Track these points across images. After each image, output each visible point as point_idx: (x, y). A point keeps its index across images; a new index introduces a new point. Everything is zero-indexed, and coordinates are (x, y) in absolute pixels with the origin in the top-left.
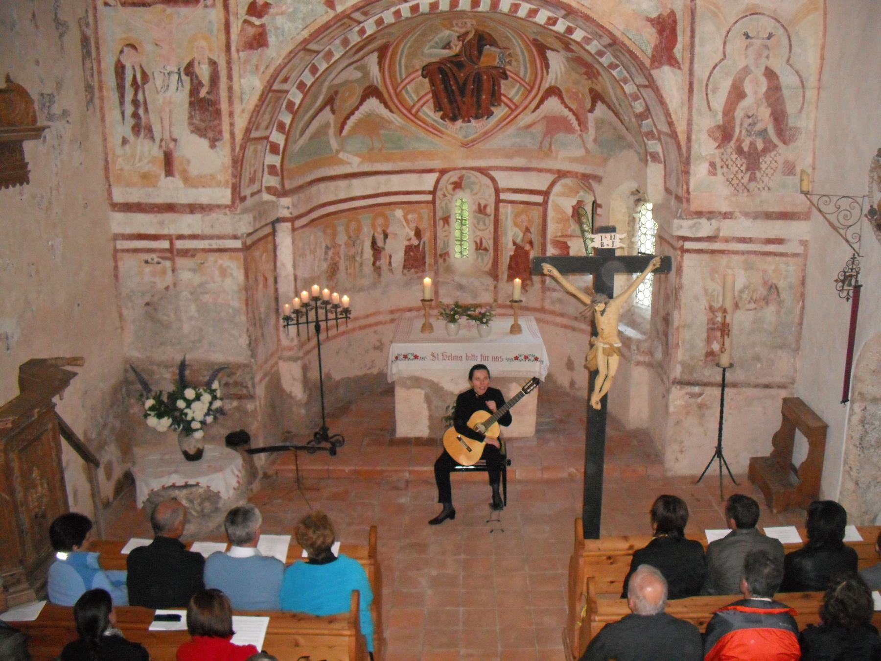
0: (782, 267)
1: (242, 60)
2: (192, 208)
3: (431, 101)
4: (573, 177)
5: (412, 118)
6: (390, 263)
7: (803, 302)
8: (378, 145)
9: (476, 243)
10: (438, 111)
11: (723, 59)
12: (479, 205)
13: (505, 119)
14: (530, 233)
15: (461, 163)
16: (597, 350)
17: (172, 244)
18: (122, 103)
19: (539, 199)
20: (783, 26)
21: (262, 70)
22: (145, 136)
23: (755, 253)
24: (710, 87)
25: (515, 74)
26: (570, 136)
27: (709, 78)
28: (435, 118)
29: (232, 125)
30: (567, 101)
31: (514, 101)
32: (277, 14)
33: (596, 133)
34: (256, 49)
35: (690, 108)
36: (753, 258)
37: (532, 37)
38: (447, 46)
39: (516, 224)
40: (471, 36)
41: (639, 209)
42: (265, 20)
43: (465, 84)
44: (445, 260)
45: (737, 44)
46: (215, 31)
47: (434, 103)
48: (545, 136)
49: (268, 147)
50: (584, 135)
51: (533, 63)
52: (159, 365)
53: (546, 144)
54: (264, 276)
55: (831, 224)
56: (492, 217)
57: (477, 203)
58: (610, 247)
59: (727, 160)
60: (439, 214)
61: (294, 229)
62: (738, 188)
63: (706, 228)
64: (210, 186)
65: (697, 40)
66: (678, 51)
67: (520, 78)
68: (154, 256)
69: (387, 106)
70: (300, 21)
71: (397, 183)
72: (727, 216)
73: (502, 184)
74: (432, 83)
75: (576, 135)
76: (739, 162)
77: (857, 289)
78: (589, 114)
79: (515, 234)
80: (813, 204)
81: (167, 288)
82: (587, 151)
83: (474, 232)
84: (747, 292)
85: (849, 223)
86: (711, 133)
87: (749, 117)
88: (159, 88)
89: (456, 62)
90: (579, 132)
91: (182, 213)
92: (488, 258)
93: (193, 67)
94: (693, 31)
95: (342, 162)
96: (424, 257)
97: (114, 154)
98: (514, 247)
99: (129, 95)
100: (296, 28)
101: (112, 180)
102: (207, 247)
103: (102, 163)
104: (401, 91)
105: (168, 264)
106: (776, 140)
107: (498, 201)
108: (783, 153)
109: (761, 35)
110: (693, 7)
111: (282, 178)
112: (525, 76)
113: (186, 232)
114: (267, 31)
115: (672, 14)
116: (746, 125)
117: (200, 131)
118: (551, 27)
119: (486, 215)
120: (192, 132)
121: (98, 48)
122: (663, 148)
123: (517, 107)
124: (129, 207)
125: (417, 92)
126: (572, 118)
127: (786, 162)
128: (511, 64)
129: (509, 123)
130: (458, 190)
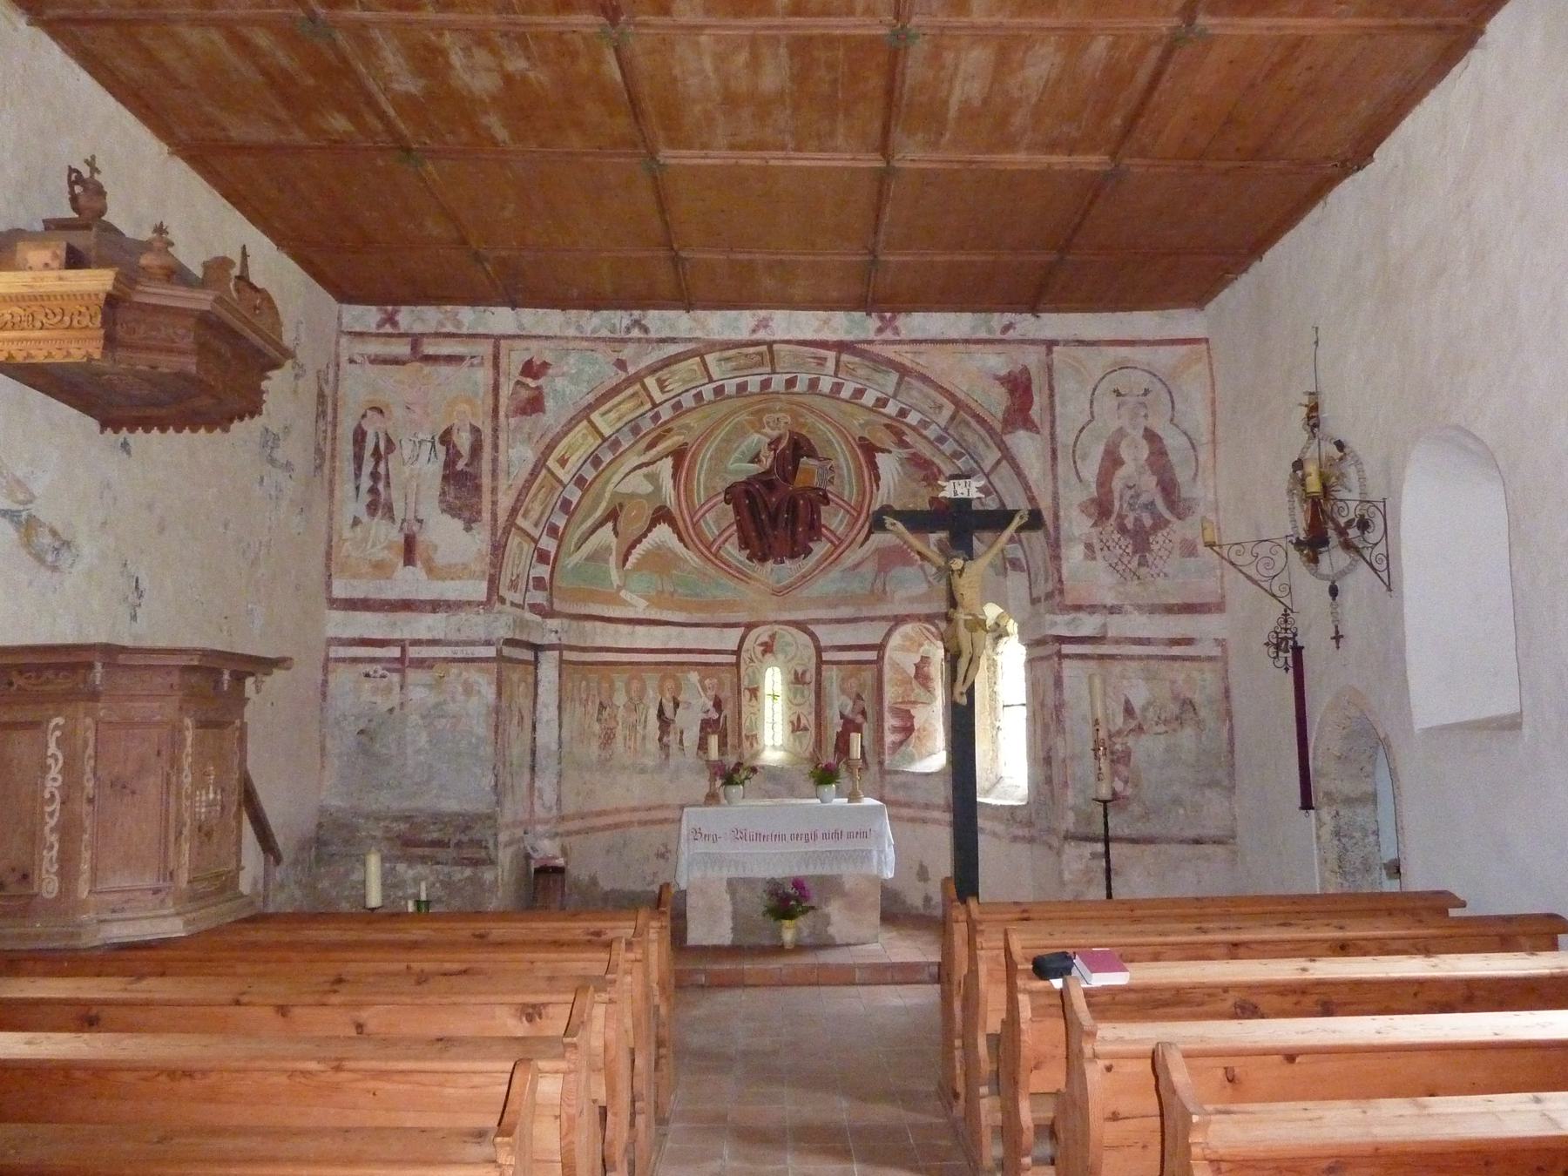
0: (1195, 674)
1: (512, 427)
2: (435, 606)
5: (712, 557)
7: (1231, 721)
8: (669, 588)
9: (792, 723)
11: (1091, 421)
12: (796, 673)
15: (772, 616)
16: (957, 623)
17: (403, 651)
18: (358, 475)
19: (871, 655)
20: (1160, 380)
21: (535, 440)
22: (384, 515)
23: (1156, 657)
24: (1078, 453)
25: (837, 497)
27: (1076, 443)
28: (742, 559)
29: (494, 503)
31: (838, 533)
35: (1055, 478)
36: (1153, 664)
37: (859, 433)
38: (756, 459)
39: (843, 691)
42: (541, 382)
43: (778, 509)
44: (752, 745)
45: (1107, 403)
46: (481, 394)
49: (535, 555)
51: (860, 476)
52: (367, 817)
53: (879, 584)
54: (520, 712)
55: (1249, 577)
56: (813, 684)
57: (793, 672)
58: (965, 496)
59: (1108, 541)
60: (745, 682)
61: (562, 661)
62: (1125, 575)
63: (1088, 625)
64: (460, 578)
65: (1057, 399)
66: (1035, 412)
67: (845, 502)
68: (378, 667)
69: (681, 539)
70: (585, 384)
71: (691, 638)
72: (1113, 610)
73: (825, 641)
74: (737, 512)
75: (916, 567)
76: (1123, 542)
77: (1298, 651)
80: (1223, 558)
81: (391, 710)
83: (790, 709)
84: (1151, 709)
85: (1272, 573)
86: (1084, 509)
87: (1130, 488)
88: (406, 458)
89: (765, 481)
90: (920, 562)
91: (421, 611)
94: (1051, 389)
95: (624, 603)
97: (340, 537)
99: (368, 467)
101: (333, 570)
102: (450, 655)
103: (323, 547)
104: (699, 520)
105: (395, 678)
106: (1167, 515)
107: (820, 663)
108: (1179, 530)
109: (1136, 392)
111: (551, 594)
113: (424, 635)
115: (1025, 370)
116: (1127, 497)
117: (451, 510)
119: (804, 683)
120: (443, 511)
121: (335, 410)
122: (1025, 552)
123: (841, 541)
124: (352, 605)
125: (717, 522)
127: (1184, 541)
128: (832, 483)
130: (768, 655)
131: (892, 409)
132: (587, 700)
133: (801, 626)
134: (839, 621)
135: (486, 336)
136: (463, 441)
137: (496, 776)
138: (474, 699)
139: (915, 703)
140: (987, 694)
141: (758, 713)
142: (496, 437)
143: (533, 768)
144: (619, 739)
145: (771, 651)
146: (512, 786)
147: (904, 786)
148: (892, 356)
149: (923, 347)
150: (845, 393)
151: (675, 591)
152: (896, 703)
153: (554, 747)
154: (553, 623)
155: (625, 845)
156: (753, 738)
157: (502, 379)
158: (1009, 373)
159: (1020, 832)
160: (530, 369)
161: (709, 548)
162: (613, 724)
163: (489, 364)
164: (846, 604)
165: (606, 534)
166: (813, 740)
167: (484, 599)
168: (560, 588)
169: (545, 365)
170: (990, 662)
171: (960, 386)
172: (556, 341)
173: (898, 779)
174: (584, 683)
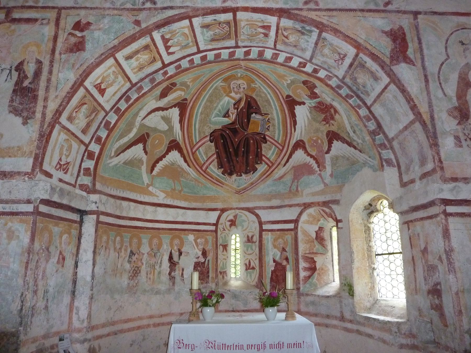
1: (63, 60)
3: (216, 160)
4: (316, 206)
5: (203, 173)
6: (182, 274)
8: (178, 188)
9: (246, 264)
10: (220, 168)
11: (446, 60)
12: (248, 237)
13: (265, 174)
14: (286, 251)
15: (235, 205)
19: (291, 226)
21: (76, 68)
24: (441, 78)
26: (312, 177)
28: (219, 173)
29: (45, 107)
30: (309, 149)
31: (271, 160)
32: (95, 30)
33: (332, 168)
34: (75, 53)
35: (428, 93)
37: (286, 92)
38: (226, 115)
39: (275, 247)
40: (242, 104)
41: (372, 220)
44: (223, 277)
45: (454, 49)
47: (218, 162)
48: (293, 182)
50: (323, 173)
53: (294, 187)
56: (257, 243)
57: (246, 236)
60: (220, 241)
61: (98, 222)
65: (424, 46)
66: (410, 52)
69: (186, 161)
71: (190, 216)
73: (263, 219)
74: (216, 147)
78: (327, 156)
79: (274, 253)
82: (326, 185)
83: (244, 256)
86: (450, 113)
90: (319, 172)
92: (255, 274)
93: (22, 65)
95: (151, 194)
96: (208, 272)
98: (275, 264)
100: (109, 39)
104: (195, 151)
107: (261, 230)
110: (417, 24)
112: (278, 138)
114: (86, 40)
115: (401, 28)
117: (15, 111)
118: (302, 69)
119: (253, 242)
120: (10, 112)
123: (273, 164)
125: (206, 154)
126: (312, 162)
128: (269, 130)
129: (268, 176)
130: (233, 227)
131: (309, 68)
132: (120, 249)
133: (251, 210)
134: (272, 208)
135: (53, 8)
136: (30, 69)
137: (22, 302)
138: (14, 243)
139: (316, 253)
140: (365, 248)
141: (227, 258)
142: (51, 66)
143: (73, 293)
144: (143, 273)
145: (235, 225)
146: (46, 308)
147: (313, 303)
148: (315, 18)
149: (335, 13)
150: (281, 59)
151: (182, 190)
152: (306, 254)
153: (89, 278)
154: (94, 197)
155: (144, 340)
156: (224, 273)
157: (60, 32)
158: (391, 29)
159: (404, 341)
160: (78, 26)
161: (201, 168)
162: (140, 264)
163: (53, 24)
164: (276, 198)
165: (138, 150)
166: (257, 275)
167: (30, 171)
168: (102, 177)
169: (89, 24)
170: (366, 228)
171: (361, 37)
172: (96, 10)
173: (309, 299)
174: (118, 238)
